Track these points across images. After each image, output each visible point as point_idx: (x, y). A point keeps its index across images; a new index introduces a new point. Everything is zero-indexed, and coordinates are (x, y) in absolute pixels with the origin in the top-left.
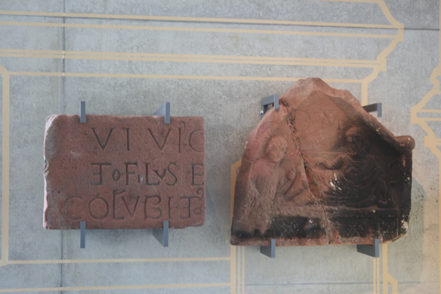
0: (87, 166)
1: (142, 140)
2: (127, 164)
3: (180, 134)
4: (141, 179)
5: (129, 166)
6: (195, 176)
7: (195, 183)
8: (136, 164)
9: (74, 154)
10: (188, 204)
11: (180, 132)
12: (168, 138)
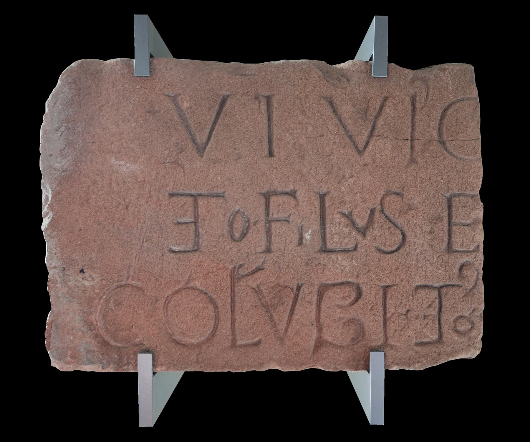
0: (158, 199)
1: (310, 128)
2: (267, 197)
3: (414, 110)
4: (307, 236)
5: (273, 199)
6: (454, 228)
7: (456, 247)
8: (292, 194)
9: (120, 165)
10: (436, 305)
11: (414, 105)
12: (380, 123)
